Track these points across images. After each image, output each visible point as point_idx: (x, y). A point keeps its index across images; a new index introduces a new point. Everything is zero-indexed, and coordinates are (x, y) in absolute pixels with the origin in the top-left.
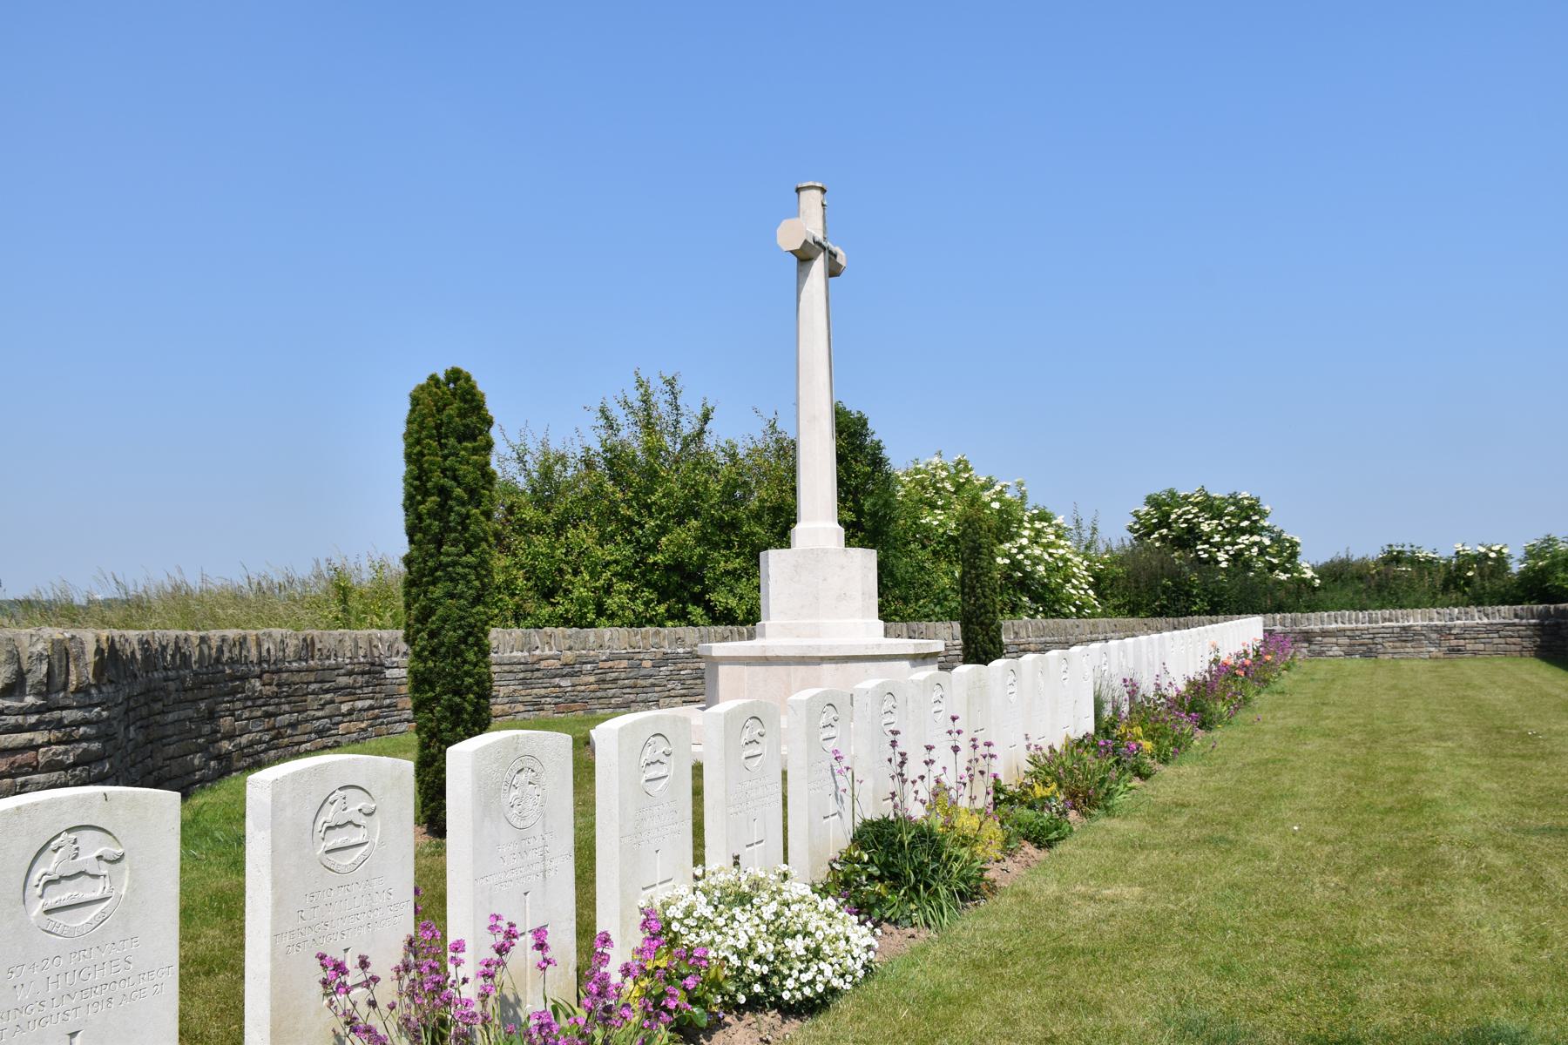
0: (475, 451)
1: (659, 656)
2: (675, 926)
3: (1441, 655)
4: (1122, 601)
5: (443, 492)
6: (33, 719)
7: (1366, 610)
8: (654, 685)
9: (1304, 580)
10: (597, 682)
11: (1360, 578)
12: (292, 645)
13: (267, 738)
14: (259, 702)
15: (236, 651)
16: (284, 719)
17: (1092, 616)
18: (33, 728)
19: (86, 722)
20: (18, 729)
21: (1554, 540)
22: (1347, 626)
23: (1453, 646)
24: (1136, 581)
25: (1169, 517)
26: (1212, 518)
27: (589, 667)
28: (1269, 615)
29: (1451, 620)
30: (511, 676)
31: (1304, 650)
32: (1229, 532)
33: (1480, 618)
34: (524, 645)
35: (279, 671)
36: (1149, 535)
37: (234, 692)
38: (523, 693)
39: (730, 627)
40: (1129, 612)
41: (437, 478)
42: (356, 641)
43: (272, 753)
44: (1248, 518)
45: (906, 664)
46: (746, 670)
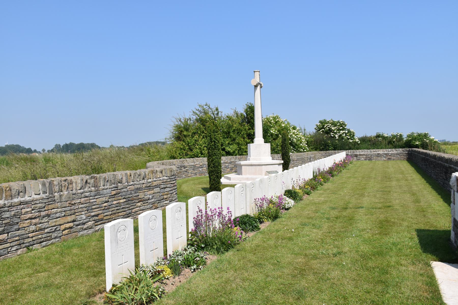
3: (386, 160)
5: (214, 142)
7: (370, 149)
11: (370, 141)
17: (307, 151)
22: (365, 153)
23: (389, 158)
24: (317, 142)
26: (334, 127)
28: (348, 151)
29: (389, 152)
31: (356, 159)
36: (319, 130)
39: (231, 156)
40: (315, 149)
41: (214, 139)
44: (342, 126)
45: (277, 165)
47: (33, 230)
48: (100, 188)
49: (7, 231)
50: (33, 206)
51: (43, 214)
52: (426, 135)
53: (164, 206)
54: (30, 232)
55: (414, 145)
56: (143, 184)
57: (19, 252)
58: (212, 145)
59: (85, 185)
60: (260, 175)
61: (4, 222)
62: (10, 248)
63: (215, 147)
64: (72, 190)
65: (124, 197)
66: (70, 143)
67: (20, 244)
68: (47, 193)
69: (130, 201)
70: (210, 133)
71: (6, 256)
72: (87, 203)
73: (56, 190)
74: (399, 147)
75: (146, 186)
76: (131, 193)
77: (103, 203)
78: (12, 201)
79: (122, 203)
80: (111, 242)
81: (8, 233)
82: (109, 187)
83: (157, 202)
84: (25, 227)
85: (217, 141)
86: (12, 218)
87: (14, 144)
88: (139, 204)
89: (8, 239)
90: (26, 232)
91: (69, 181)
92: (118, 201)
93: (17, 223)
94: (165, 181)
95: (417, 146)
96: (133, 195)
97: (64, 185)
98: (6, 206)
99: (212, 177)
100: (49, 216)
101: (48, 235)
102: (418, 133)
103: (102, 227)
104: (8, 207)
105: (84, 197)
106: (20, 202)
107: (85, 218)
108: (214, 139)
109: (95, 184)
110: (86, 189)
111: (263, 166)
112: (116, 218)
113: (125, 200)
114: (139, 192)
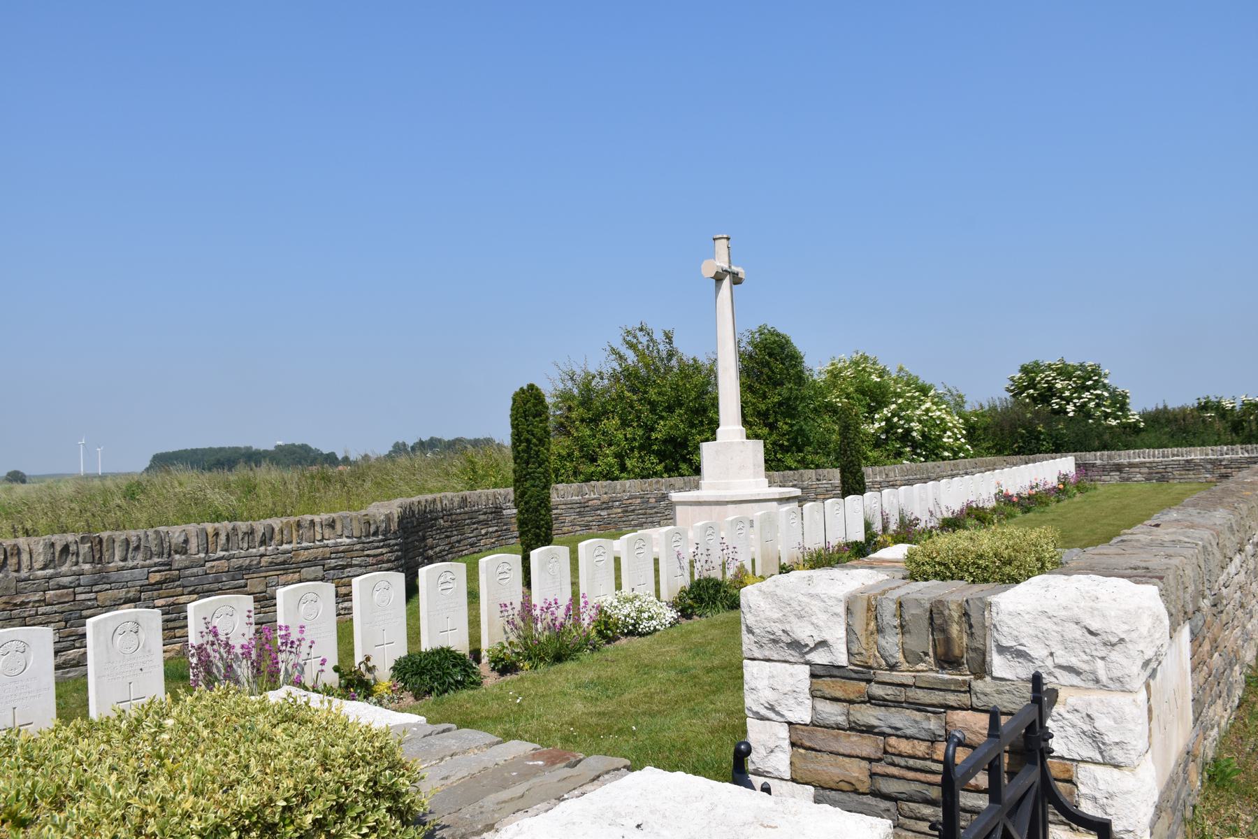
0: (541, 421)
2: (605, 609)
3: (1214, 479)
4: (991, 444)
5: (528, 441)
6: (382, 544)
8: (657, 513)
10: (623, 512)
11: (1169, 421)
12: (457, 500)
13: (447, 548)
14: (443, 531)
15: (432, 506)
16: (454, 539)
18: (382, 547)
19: (396, 544)
20: (378, 548)
22: (1147, 460)
25: (1035, 380)
27: (617, 503)
29: (1222, 455)
30: (572, 511)
31: (1117, 477)
32: (1076, 390)
33: (1243, 454)
34: (579, 492)
35: (451, 514)
37: (432, 526)
38: (579, 519)
41: (525, 435)
42: (487, 496)
43: (450, 556)
44: (1090, 379)
45: (775, 504)
48: (110, 565)
75: (271, 563)
87: (297, 444)
92: (171, 599)
94: (341, 548)
96: (224, 585)
105: (56, 587)
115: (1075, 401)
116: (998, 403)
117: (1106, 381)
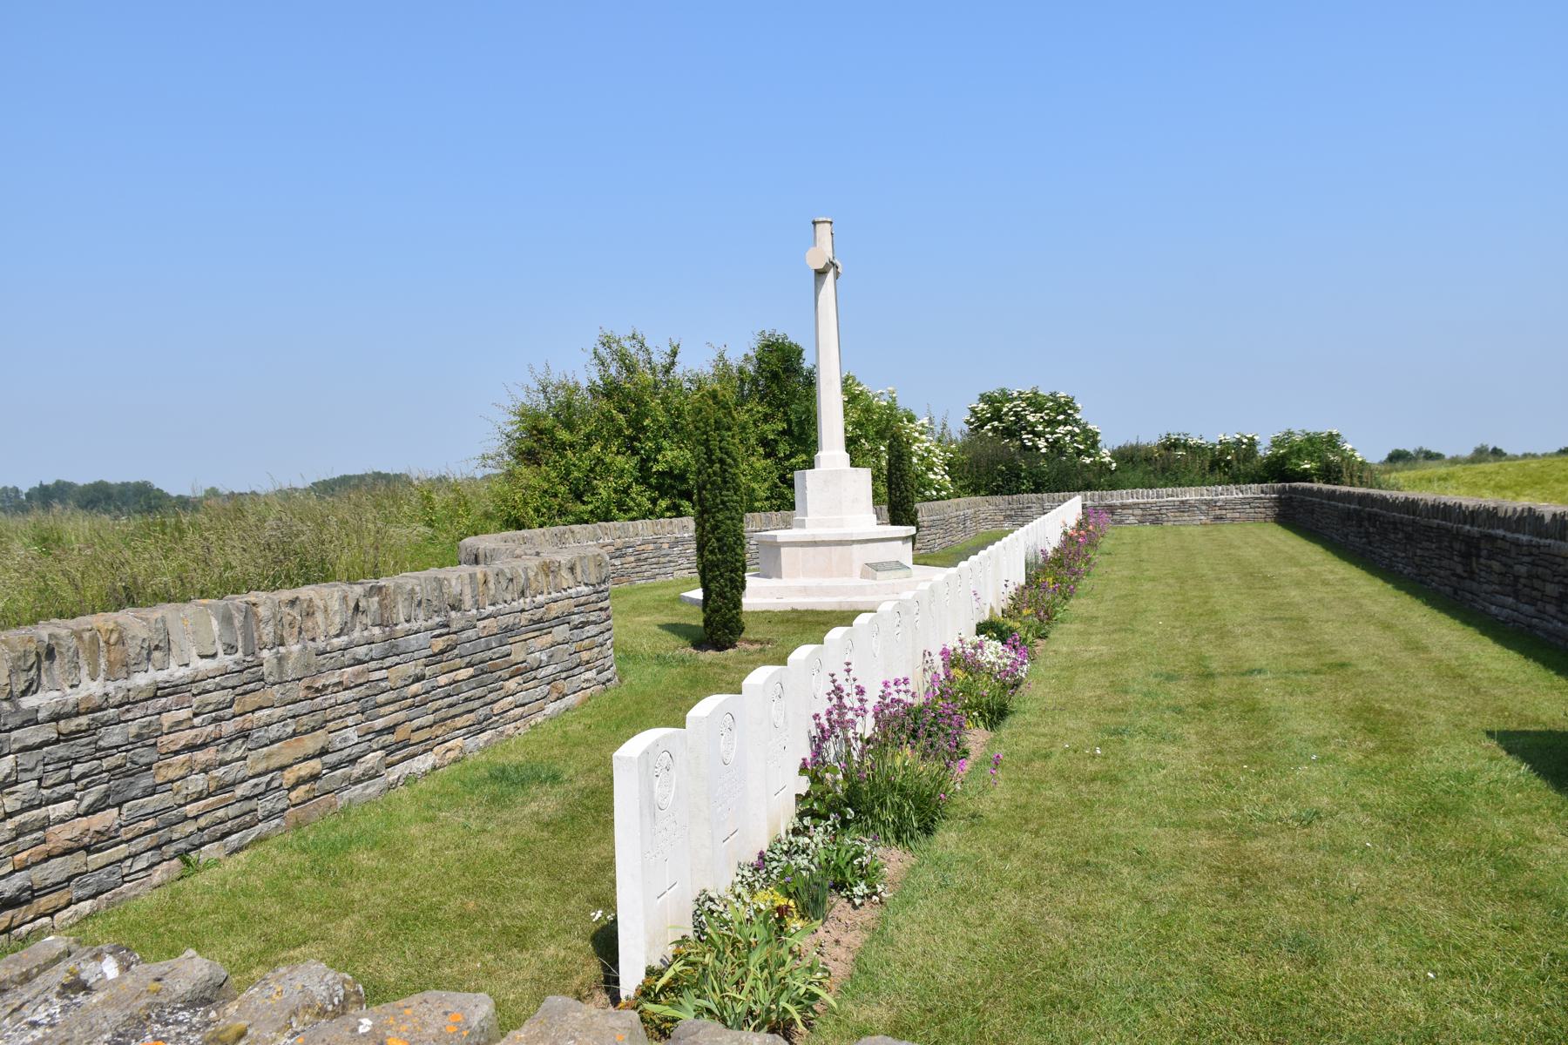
1: (673, 540)
3: (1208, 522)
4: (966, 482)
5: (722, 461)
8: (670, 562)
9: (1103, 464)
21: (1292, 433)
22: (1141, 501)
23: (1218, 515)
26: (1035, 412)
27: (631, 550)
29: (1217, 495)
36: (982, 427)
44: (1064, 412)
45: (900, 542)
46: (800, 550)
47: (200, 789)
49: (118, 799)
50: (196, 701)
51: (228, 728)
52: (1332, 441)
53: (583, 689)
54: (189, 800)
55: (1298, 473)
56: (523, 611)
57: (158, 875)
58: (715, 473)
59: (352, 617)
60: (846, 575)
61: (106, 764)
62: (128, 862)
63: (725, 482)
64: (313, 640)
65: (467, 659)
66: (58, 483)
67: (159, 847)
68: (237, 651)
69: (486, 673)
70: (705, 433)
71: (115, 894)
72: (361, 685)
73: (265, 638)
74: (1248, 480)
76: (488, 645)
77: (407, 683)
78: (129, 684)
79: (463, 680)
80: (641, 815)
81: (119, 805)
82: (424, 623)
83: (564, 675)
84: (172, 781)
85: (729, 461)
86: (130, 747)
88: (512, 685)
89: (121, 826)
90: (178, 797)
91: (305, 606)
93: (149, 766)
94: (582, 600)
95: (1307, 477)
96: (494, 653)
97: (289, 618)
98: (111, 701)
99: (713, 586)
100: (247, 737)
101: (247, 806)
102: (1307, 434)
103: (407, 772)
104: (117, 707)
105: (352, 662)
106: (153, 688)
107: (356, 741)
108: (718, 453)
109: (382, 615)
110: (356, 635)
111: (855, 547)
112: (447, 737)
113: (471, 671)
114: (511, 640)
115: (1048, 436)
116: (509, 429)
117: (1078, 416)
